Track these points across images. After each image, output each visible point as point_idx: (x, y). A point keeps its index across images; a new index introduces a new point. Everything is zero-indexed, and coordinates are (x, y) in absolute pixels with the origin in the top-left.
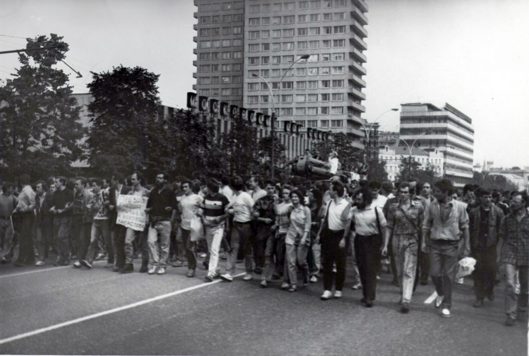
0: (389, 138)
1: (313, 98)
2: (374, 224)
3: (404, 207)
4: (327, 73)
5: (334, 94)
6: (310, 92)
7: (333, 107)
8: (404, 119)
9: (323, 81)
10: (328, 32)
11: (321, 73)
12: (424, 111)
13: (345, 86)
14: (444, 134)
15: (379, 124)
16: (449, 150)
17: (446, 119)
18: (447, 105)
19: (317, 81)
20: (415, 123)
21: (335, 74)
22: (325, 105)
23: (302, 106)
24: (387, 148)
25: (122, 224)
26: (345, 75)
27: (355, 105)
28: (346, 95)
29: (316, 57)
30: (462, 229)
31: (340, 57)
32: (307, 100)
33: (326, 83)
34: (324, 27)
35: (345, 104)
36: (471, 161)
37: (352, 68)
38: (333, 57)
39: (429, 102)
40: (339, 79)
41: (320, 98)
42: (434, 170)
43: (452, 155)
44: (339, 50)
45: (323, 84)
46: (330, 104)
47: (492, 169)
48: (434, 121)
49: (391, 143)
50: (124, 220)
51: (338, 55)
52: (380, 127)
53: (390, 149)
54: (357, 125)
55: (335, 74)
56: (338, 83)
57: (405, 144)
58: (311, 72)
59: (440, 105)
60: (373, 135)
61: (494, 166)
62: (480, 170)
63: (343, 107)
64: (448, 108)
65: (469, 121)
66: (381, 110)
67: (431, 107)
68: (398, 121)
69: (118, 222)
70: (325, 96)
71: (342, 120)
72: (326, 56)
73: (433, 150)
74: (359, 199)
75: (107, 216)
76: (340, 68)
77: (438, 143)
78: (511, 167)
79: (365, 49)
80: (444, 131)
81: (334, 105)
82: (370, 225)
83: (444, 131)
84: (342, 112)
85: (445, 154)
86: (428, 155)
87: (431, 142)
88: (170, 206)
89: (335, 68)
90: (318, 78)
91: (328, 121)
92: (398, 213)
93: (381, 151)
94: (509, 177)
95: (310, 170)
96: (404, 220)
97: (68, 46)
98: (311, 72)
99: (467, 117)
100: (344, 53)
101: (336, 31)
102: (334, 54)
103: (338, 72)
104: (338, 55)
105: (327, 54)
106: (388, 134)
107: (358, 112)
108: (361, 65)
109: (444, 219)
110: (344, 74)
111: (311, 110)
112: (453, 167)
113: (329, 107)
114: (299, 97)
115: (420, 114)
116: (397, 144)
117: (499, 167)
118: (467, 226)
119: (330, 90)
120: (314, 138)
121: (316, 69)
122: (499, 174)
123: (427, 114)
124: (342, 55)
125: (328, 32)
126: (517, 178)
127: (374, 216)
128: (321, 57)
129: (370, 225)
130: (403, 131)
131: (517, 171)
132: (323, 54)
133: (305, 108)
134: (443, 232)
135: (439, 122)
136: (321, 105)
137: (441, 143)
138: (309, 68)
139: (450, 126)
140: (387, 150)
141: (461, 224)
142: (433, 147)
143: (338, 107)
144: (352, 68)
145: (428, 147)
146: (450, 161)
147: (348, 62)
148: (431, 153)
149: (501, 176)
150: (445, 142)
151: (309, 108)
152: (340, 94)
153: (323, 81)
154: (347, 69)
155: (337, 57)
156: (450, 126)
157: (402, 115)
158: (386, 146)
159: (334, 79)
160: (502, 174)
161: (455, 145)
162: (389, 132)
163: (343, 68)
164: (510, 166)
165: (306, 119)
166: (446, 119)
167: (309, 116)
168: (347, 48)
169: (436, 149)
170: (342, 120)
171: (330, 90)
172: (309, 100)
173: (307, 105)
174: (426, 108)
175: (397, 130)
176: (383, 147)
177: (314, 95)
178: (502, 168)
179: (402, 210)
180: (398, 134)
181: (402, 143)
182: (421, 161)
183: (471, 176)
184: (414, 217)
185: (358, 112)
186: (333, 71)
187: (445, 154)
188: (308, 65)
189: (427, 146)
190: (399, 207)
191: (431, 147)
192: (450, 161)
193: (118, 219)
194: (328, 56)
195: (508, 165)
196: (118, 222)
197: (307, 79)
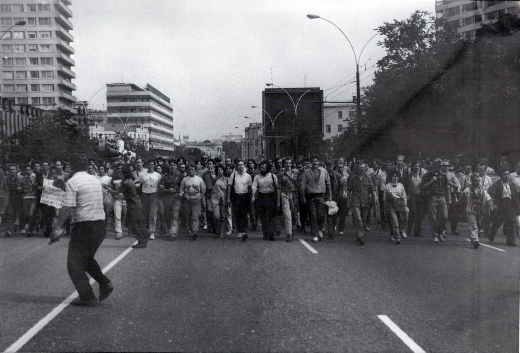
0: (96, 116)
1: (22, 76)
2: (271, 186)
3: (288, 173)
4: (34, 50)
5: (43, 72)
6: (19, 69)
7: (43, 85)
8: (110, 98)
9: (31, 59)
10: (32, 10)
11: (28, 50)
12: (128, 91)
13: (54, 63)
14: (148, 112)
15: (88, 103)
16: (152, 126)
17: (148, 98)
18: (149, 85)
19: (25, 58)
20: (121, 102)
21: (44, 52)
22: (35, 82)
23: (10, 82)
24: (97, 125)
25: (45, 203)
26: (53, 53)
27: (65, 82)
28: (56, 74)
29: (21, 34)
30: (327, 185)
31: (47, 35)
32: (15, 77)
33: (34, 61)
34: (28, 5)
35: (56, 81)
36: (171, 136)
37: (60, 47)
38: (39, 35)
39: (132, 83)
40: (48, 57)
41: (29, 75)
42: (145, 145)
43: (156, 131)
44: (46, 28)
45: (31, 62)
46: (40, 81)
47: (188, 143)
48: (138, 100)
49: (100, 121)
50: (47, 200)
51: (44, 33)
52: (89, 105)
53: (99, 125)
54: (69, 102)
55: (43, 52)
56: (47, 60)
57: (120, 121)
58: (18, 49)
59: (142, 85)
60: (82, 113)
61: (190, 140)
62: (178, 144)
63: (53, 85)
64: (149, 88)
65: (168, 100)
66: (90, 90)
67: (134, 87)
68: (105, 100)
69: (41, 201)
70: (34, 74)
71: (54, 98)
72: (32, 33)
73: (139, 127)
74: (264, 168)
75: (35, 196)
76: (48, 46)
77: (143, 120)
78: (203, 141)
79: (72, 29)
80: (148, 109)
81: (45, 82)
82: (269, 186)
83: (148, 109)
84: (54, 90)
85: (150, 130)
86: (135, 131)
87: (136, 119)
88: (470, 165)
89: (42, 45)
90: (25, 56)
91: (39, 98)
92: (285, 178)
93: (91, 128)
94: (204, 149)
95: (109, 150)
96: (289, 181)
97: (319, 88)
98: (18, 49)
99: (165, 96)
100: (51, 32)
101: (40, 10)
102: (40, 31)
103: (46, 50)
104: (44, 33)
105: (33, 32)
106: (96, 112)
107: (69, 90)
108: (68, 44)
109: (317, 180)
110: (52, 52)
111: (20, 87)
112: (158, 141)
113: (39, 85)
114: (7, 74)
115: (125, 94)
116: (105, 122)
117: (194, 141)
118: (329, 183)
119: (39, 68)
120: (33, 115)
121: (23, 46)
122: (194, 147)
123: (132, 94)
124: (49, 33)
125: (32, 10)
126: (209, 150)
127: (271, 180)
128: (27, 34)
129: (269, 186)
130: (111, 109)
131: (208, 144)
132: (29, 32)
133: (14, 85)
134: (317, 189)
135: (143, 101)
136: (31, 82)
137: (146, 120)
138: (16, 45)
139: (153, 105)
140: (97, 127)
141: (326, 182)
142: (139, 124)
143: (48, 85)
144: (60, 47)
145: (134, 124)
146: (154, 136)
147: (54, 41)
148: (138, 129)
149: (197, 149)
150: (150, 119)
151: (18, 85)
152: (50, 71)
153: (31, 59)
154: (55, 47)
155: (43, 35)
156: (153, 105)
157: (108, 95)
158: (96, 123)
159: (43, 56)
160: (197, 147)
161: (157, 122)
162: (96, 111)
163: (51, 46)
164: (203, 140)
165: (16, 96)
166: (148, 98)
167: (18, 93)
168: (55, 27)
169: (142, 125)
170: (54, 98)
171: (39, 68)
172: (17, 77)
173: (16, 82)
174: (130, 88)
175: (105, 109)
176: (93, 125)
177: (22, 72)
178: (196, 142)
179: (287, 175)
180: (105, 113)
181: (110, 120)
182: (133, 137)
183: (172, 149)
184: (295, 179)
185: (69, 90)
186: (40, 48)
187: (150, 130)
188: (13, 42)
189: (133, 123)
190: (284, 174)
191: (137, 124)
192: (154, 136)
193: (42, 199)
194: (34, 34)
195: (201, 139)
196: (41, 201)
197: (14, 56)
